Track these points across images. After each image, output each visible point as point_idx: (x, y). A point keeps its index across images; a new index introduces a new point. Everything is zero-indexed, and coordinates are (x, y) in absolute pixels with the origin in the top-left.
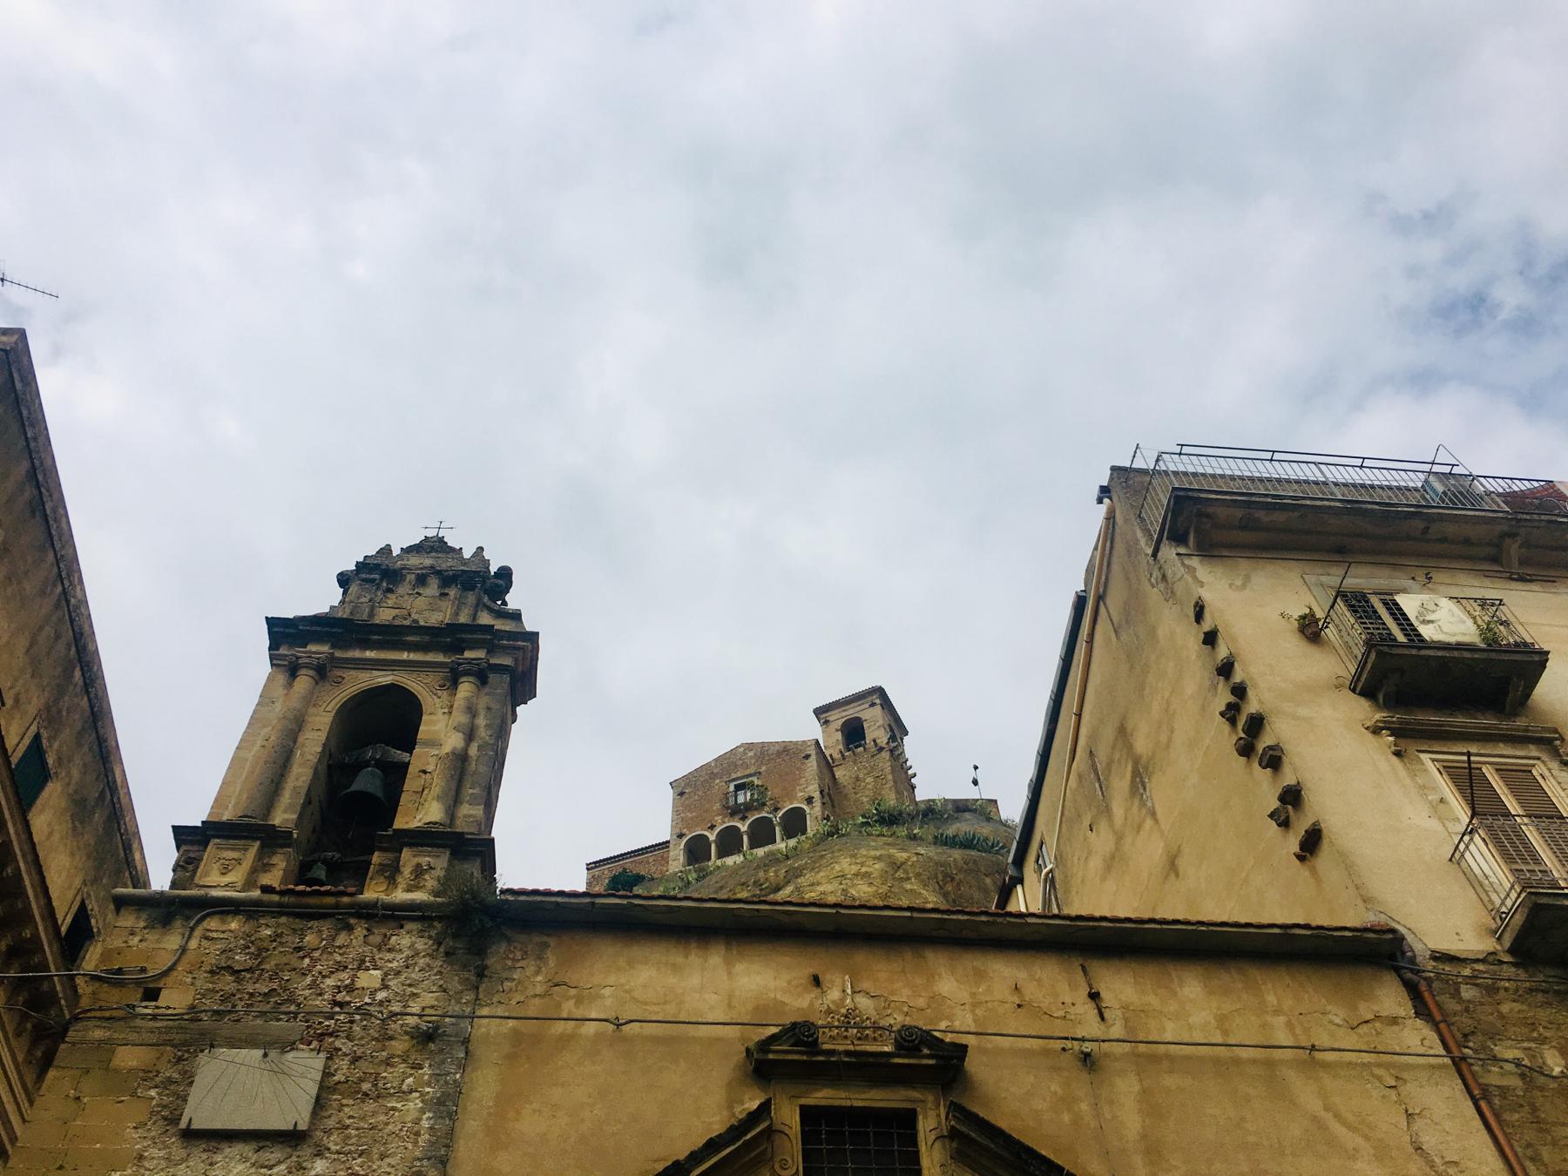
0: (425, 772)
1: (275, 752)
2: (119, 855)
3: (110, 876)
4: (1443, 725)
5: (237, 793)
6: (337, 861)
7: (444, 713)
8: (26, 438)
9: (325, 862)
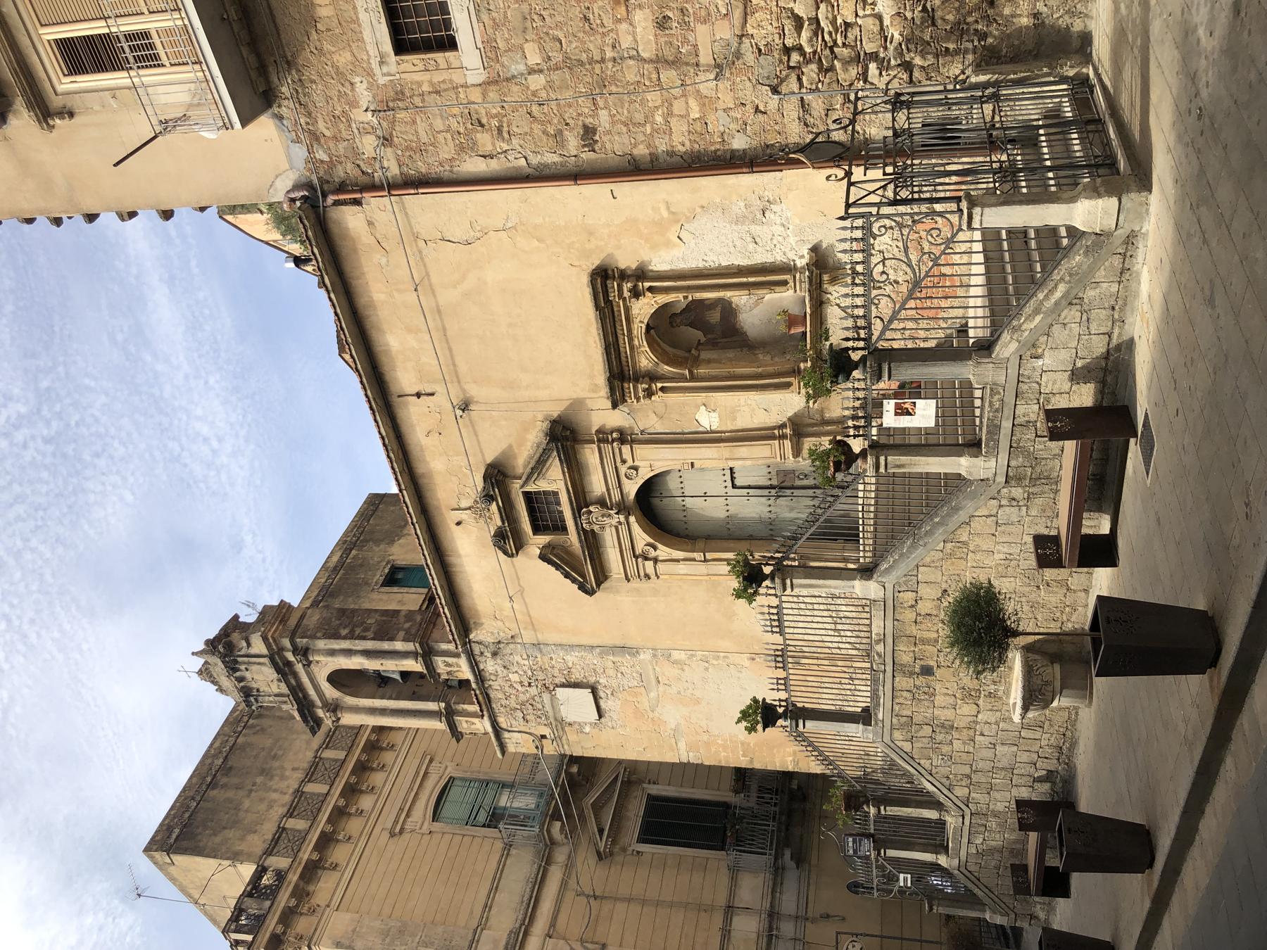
2: (344, 574)
3: (357, 574)
4: (15, 70)
8: (198, 804)
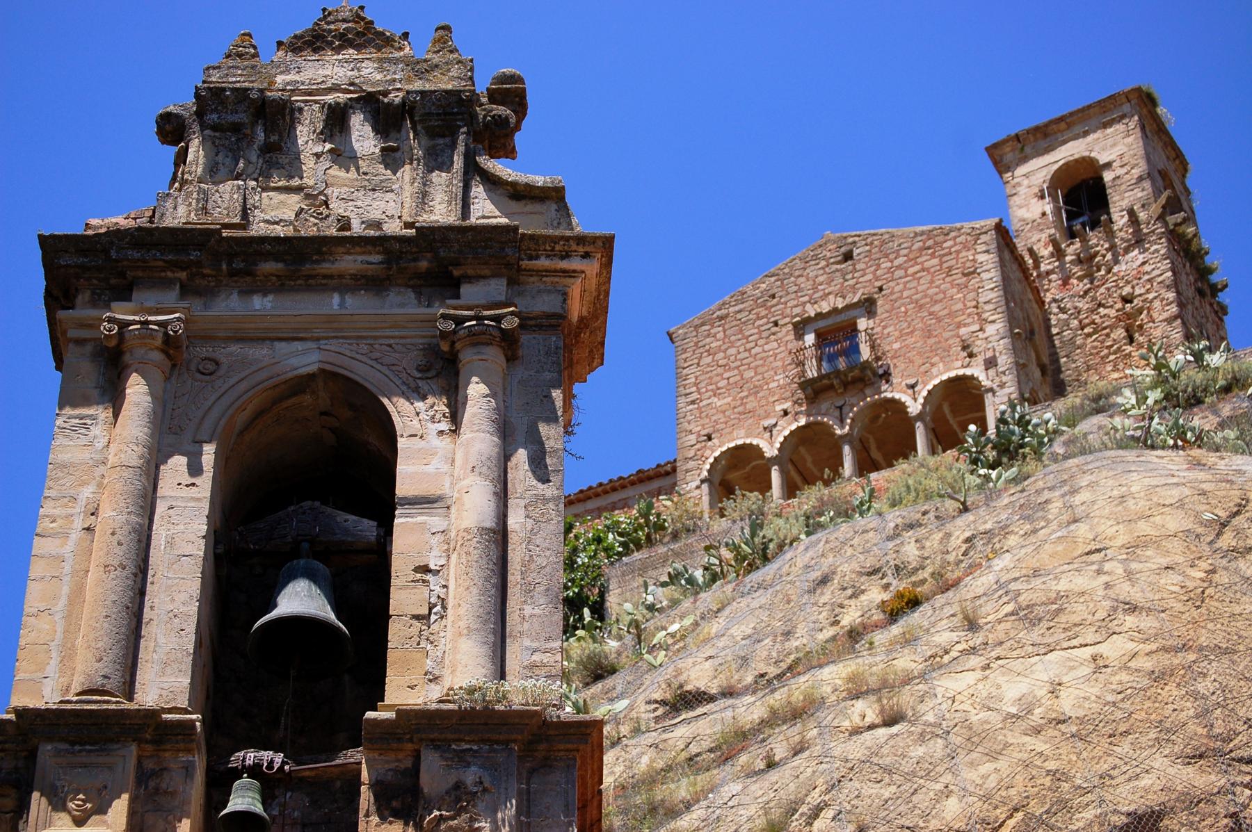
0: (425, 569)
1: (119, 544)
5: (59, 635)
6: (281, 768)
7: (441, 432)
9: (255, 771)
